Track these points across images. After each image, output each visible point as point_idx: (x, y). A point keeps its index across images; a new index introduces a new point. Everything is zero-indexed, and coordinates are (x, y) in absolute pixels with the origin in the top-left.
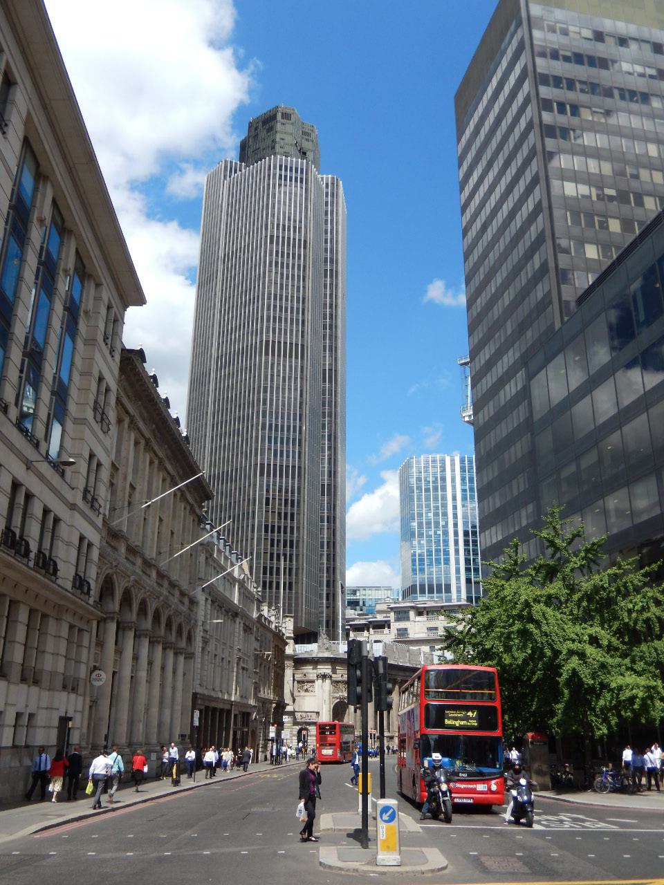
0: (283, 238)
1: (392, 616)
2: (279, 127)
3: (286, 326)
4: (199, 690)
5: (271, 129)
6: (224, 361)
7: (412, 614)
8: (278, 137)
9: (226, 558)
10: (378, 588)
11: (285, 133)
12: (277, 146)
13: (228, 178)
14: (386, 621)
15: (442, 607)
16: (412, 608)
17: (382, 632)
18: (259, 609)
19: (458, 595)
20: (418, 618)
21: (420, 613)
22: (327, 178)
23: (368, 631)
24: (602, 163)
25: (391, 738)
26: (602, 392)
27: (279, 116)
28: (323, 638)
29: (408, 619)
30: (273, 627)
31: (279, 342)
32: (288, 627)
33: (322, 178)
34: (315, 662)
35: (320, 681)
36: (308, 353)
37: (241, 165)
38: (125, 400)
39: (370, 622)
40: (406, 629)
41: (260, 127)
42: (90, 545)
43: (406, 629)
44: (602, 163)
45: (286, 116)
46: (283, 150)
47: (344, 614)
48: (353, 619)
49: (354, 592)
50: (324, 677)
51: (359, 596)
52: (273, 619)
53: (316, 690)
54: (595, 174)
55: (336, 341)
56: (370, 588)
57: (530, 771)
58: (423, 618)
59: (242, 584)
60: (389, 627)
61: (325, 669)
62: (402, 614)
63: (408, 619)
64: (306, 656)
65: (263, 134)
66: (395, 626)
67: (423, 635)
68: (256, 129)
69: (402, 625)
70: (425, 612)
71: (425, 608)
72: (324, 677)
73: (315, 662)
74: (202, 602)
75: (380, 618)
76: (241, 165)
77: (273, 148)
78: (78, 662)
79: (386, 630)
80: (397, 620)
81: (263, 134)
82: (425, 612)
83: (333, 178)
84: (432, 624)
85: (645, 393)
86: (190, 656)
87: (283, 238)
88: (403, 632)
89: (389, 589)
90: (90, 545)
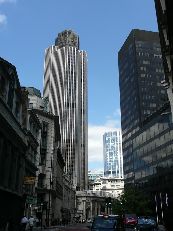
1: (101, 182)
4: (64, 207)
5: (65, 37)
7: (107, 181)
11: (69, 38)
13: (52, 52)
14: (99, 183)
15: (116, 179)
16: (107, 180)
17: (99, 186)
19: (121, 175)
20: (109, 183)
22: (82, 51)
23: (94, 186)
24: (159, 70)
25: (29, 181)
27: (67, 32)
29: (106, 183)
31: (67, 103)
33: (80, 51)
35: (83, 202)
36: (77, 106)
37: (56, 47)
39: (95, 183)
40: (105, 186)
41: (62, 35)
43: (105, 186)
44: (159, 70)
45: (70, 33)
46: (69, 43)
50: (84, 201)
53: (82, 204)
54: (158, 72)
57: (28, 203)
60: (100, 185)
62: (104, 181)
63: (106, 183)
64: (79, 195)
65: (63, 38)
66: (102, 185)
67: (110, 188)
68: (61, 36)
69: (104, 185)
70: (111, 181)
71: (111, 180)
74: (64, 188)
75: (98, 182)
76: (56, 47)
77: (66, 43)
81: (63, 38)
82: (111, 181)
83: (83, 51)
84: (113, 184)
85: (164, 134)
86: (62, 200)
88: (104, 187)
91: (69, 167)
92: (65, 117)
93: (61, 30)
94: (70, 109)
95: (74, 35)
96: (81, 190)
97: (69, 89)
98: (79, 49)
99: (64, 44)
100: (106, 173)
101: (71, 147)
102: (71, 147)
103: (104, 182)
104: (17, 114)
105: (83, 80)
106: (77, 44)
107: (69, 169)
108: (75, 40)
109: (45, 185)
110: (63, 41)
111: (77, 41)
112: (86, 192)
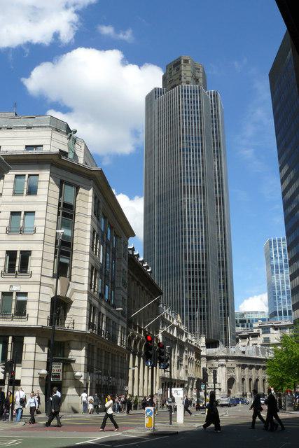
0: (191, 186)
2: (183, 68)
3: (195, 230)
5: (178, 69)
6: (161, 198)
8: (183, 73)
9: (170, 317)
10: (256, 312)
12: (183, 79)
18: (186, 336)
20: (276, 332)
21: (276, 328)
26: (297, 297)
27: (182, 61)
28: (221, 345)
30: (193, 344)
32: (202, 341)
34: (217, 358)
38: (130, 272)
40: (268, 338)
42: (103, 315)
43: (268, 338)
45: (186, 61)
46: (185, 80)
47: (233, 330)
48: (241, 333)
49: (243, 315)
50: (222, 365)
51: (246, 317)
52: (193, 340)
55: (222, 181)
56: (252, 313)
58: (278, 331)
59: (178, 327)
61: (222, 361)
62: (266, 330)
65: (174, 72)
68: (170, 69)
69: (266, 336)
72: (222, 365)
73: (217, 358)
77: (180, 79)
78: (101, 363)
79: (258, 338)
80: (264, 333)
87: (191, 186)
88: (267, 340)
89: (263, 312)
90: (103, 315)
91: (203, 289)
92: (192, 241)
93: (172, 59)
94: (194, 197)
95: (194, 65)
96: (226, 344)
97: (190, 161)
98: (206, 90)
99: (178, 82)
100: (273, 314)
101: (197, 175)
102: (197, 175)
103: (267, 330)
104: (231, 388)
105: (217, 143)
106: (201, 81)
107: (204, 293)
108: (197, 73)
109: (78, 287)
110: (175, 78)
111: (201, 75)
112: (181, 384)
